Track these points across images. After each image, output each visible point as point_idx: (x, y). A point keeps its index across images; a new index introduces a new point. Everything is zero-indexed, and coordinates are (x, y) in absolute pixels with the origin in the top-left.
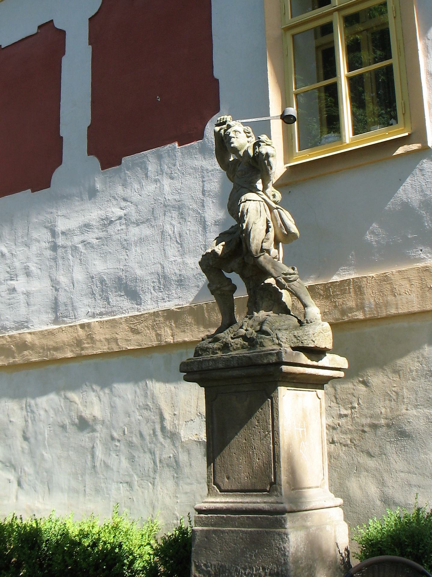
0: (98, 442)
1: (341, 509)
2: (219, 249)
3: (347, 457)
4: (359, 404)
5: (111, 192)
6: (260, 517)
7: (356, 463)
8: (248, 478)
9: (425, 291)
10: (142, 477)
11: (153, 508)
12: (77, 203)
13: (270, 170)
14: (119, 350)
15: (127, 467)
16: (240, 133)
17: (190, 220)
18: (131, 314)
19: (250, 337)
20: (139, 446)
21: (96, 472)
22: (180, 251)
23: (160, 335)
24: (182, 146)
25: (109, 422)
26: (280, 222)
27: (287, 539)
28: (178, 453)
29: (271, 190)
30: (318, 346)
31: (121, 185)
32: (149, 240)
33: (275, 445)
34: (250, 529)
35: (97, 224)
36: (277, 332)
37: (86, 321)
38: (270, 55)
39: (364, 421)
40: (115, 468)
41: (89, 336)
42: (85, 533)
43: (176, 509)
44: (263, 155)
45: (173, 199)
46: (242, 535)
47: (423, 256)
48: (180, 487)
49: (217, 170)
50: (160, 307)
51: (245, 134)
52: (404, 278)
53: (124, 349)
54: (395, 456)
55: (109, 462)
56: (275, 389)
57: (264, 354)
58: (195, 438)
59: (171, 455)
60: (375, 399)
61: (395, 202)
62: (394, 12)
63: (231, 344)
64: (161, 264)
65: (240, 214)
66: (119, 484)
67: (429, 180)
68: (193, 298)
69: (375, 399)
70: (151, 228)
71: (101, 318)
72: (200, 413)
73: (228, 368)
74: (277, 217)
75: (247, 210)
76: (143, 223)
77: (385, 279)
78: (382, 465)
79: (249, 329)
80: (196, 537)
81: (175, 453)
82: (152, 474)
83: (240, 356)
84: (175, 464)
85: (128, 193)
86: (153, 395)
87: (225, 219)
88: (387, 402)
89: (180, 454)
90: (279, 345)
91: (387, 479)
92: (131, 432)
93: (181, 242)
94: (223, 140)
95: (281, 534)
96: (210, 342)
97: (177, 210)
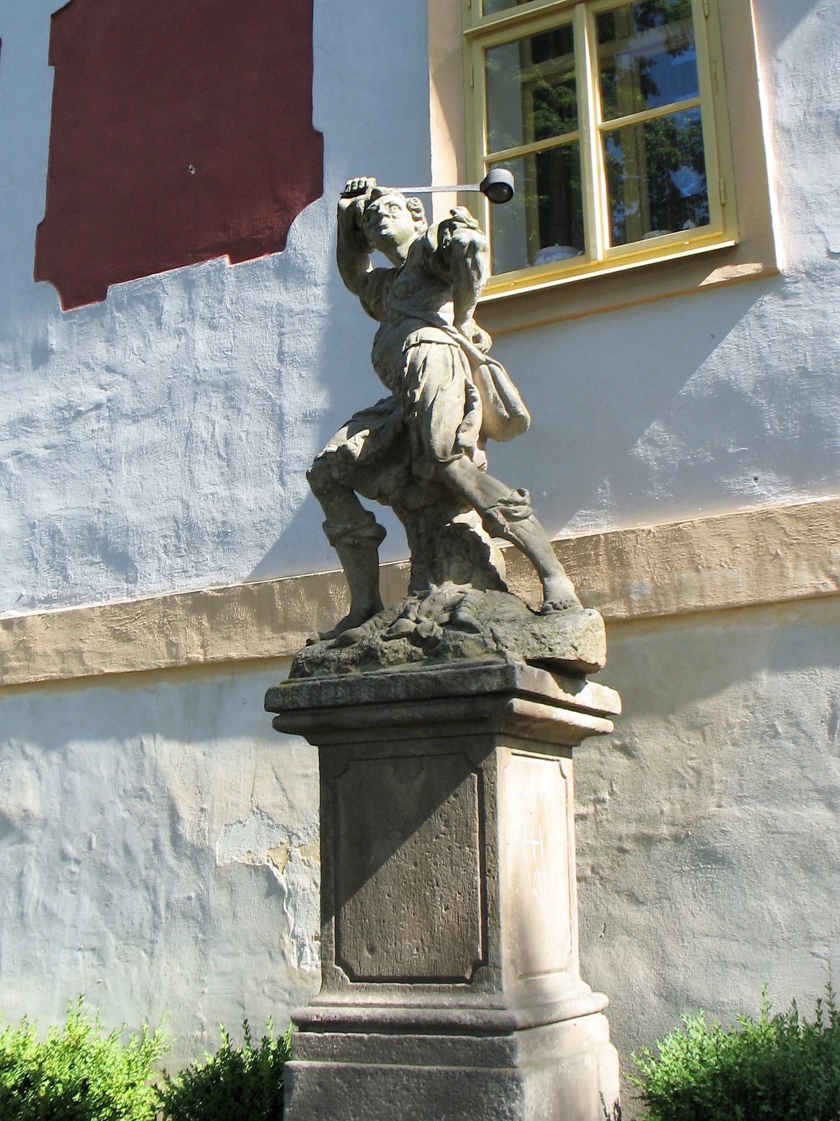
0: (32, 864)
1: (604, 1016)
2: (357, 444)
3: (583, 903)
4: (612, 793)
5: (82, 354)
6: (452, 1041)
7: (604, 915)
8: (421, 951)
9: (763, 563)
10: (127, 939)
11: (150, 1003)
12: (7, 376)
13: (476, 278)
14: (85, 674)
15: (93, 917)
16: (400, 208)
17: (248, 411)
18: (113, 602)
19: (428, 637)
20: (122, 872)
21: (25, 926)
22: (226, 473)
23: (176, 645)
24: (238, 264)
25: (58, 822)
26: (493, 390)
27: (518, 1091)
28: (207, 889)
29: (470, 326)
30: (583, 659)
31: (103, 339)
32: (157, 451)
33: (488, 878)
34: (427, 1068)
35: (48, 417)
36: (492, 624)
37: (15, 614)
38: (436, 84)
39: (623, 829)
40: (67, 919)
41: (22, 645)
42: (6, 1059)
43: (200, 1006)
44: (464, 247)
45: (213, 368)
46: (408, 1080)
47: (758, 490)
48: (212, 961)
49: (313, 312)
50: (176, 587)
51: (409, 214)
52: (719, 535)
53: (96, 673)
54: (691, 903)
55: (55, 907)
56: (490, 750)
57: (471, 673)
58: (246, 859)
59: (193, 895)
60: (649, 784)
61: (701, 381)
62: (706, 6)
63: (382, 652)
64: (182, 500)
65: (406, 369)
66: (75, 952)
67: (776, 338)
68: (251, 570)
69: (649, 784)
70: (164, 429)
71: (47, 608)
72: (257, 808)
73: (381, 703)
74: (487, 380)
75: (425, 361)
76: (146, 416)
77: (677, 535)
78: (661, 920)
79: (423, 618)
80: (293, 1083)
81: (201, 891)
82: (147, 932)
83: (411, 675)
84: (200, 914)
85: (118, 355)
86: (155, 769)
87: (325, 411)
88: (676, 790)
89: (211, 891)
90: (501, 653)
91: (674, 950)
92: (107, 845)
93: (226, 455)
94: (356, 228)
95: (504, 1080)
96: (330, 647)
97: (221, 390)
